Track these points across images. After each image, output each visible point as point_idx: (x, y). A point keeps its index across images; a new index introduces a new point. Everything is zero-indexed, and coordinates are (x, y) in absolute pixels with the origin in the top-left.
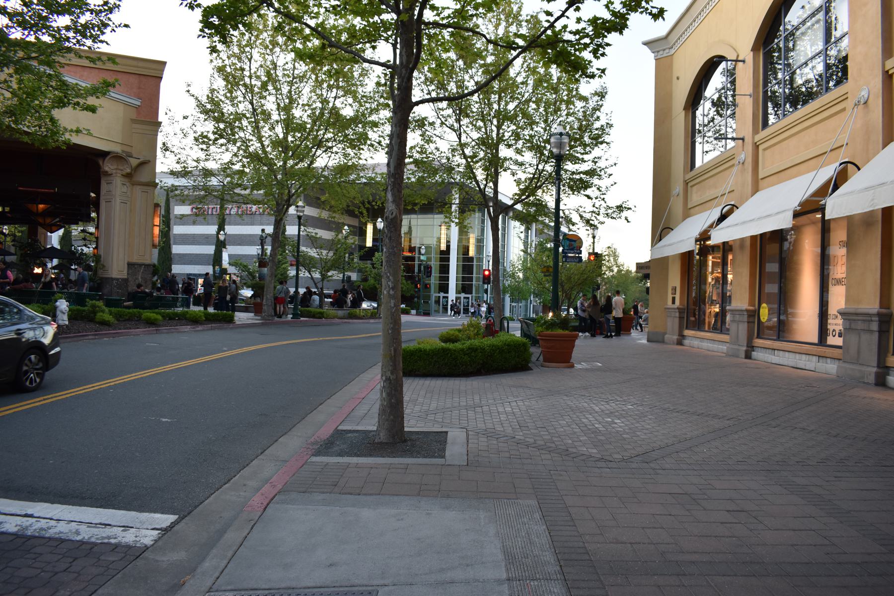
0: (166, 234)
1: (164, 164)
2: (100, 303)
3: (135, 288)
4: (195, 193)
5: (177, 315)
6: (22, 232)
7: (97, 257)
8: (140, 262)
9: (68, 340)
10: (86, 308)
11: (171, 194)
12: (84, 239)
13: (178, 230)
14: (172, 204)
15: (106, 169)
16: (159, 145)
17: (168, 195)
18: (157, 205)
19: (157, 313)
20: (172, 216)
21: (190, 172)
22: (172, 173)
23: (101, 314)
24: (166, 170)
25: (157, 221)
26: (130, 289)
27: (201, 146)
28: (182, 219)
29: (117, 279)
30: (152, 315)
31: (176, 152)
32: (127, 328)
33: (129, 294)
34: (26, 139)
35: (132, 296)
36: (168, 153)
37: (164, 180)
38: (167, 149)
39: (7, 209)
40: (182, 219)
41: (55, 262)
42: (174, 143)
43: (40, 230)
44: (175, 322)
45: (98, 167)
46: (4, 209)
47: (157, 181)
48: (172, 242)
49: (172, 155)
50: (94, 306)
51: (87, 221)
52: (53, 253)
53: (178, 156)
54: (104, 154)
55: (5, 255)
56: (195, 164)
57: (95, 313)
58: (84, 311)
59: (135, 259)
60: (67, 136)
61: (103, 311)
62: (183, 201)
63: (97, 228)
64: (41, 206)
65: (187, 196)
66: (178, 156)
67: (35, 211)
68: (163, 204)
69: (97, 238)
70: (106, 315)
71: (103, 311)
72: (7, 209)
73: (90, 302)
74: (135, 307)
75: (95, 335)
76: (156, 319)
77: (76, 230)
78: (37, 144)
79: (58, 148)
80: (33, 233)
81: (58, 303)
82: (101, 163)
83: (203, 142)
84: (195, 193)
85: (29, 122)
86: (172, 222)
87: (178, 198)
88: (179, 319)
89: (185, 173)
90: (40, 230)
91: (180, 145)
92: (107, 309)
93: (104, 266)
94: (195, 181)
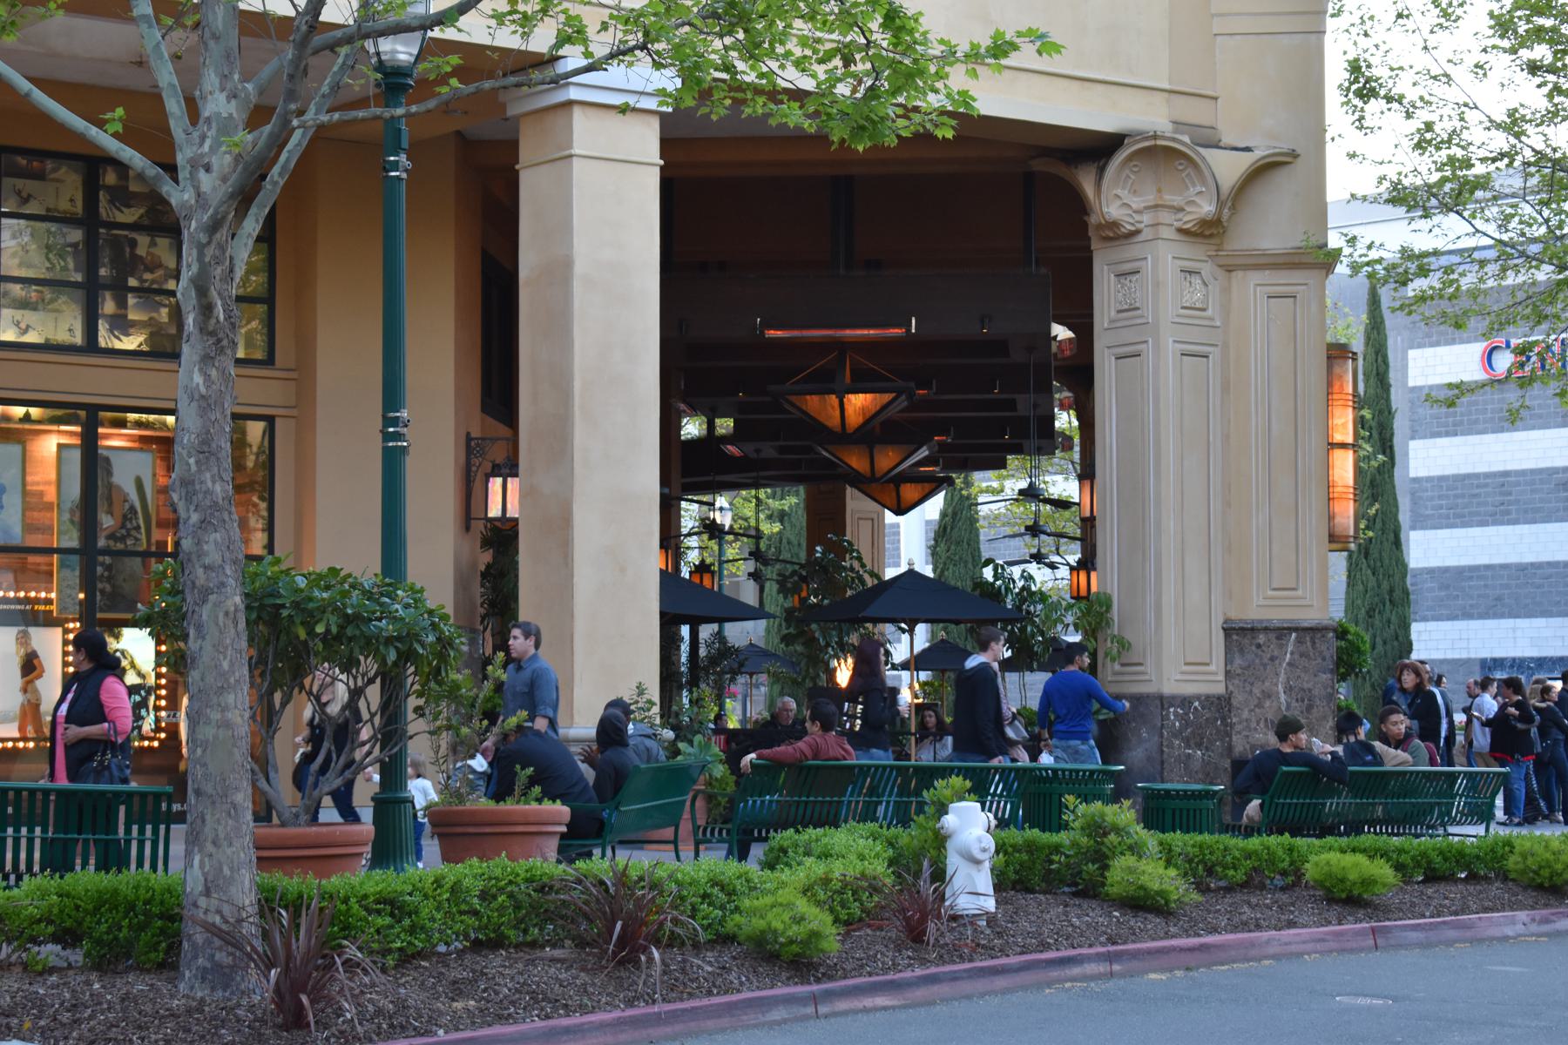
0: (1377, 484)
1: (1360, 159)
2: (1124, 814)
3: (1272, 740)
4: (1511, 280)
5: (1460, 858)
6: (782, 516)
7: (1093, 610)
8: (1278, 616)
9: (1001, 982)
10: (1063, 837)
11: (1385, 294)
12: (1034, 530)
13: (1425, 458)
14: (1394, 342)
15: (1113, 211)
16: (1335, 73)
17: (1374, 302)
18: (1337, 353)
19: (1372, 853)
20: (1397, 399)
21: (1483, 182)
22: (1403, 198)
23: (1129, 860)
24: (1370, 189)
25: (1343, 425)
26: (1240, 745)
27: (1525, 54)
28: (1451, 407)
29: (1185, 701)
30: (1349, 859)
31: (1412, 95)
32: (1244, 926)
33: (1238, 765)
34: (793, 116)
35: (1255, 774)
36: (1375, 105)
37: (1366, 234)
38: (1367, 93)
39: (725, 425)
40: (1451, 407)
41: (922, 636)
42: (1400, 54)
43: (856, 502)
44: (1454, 892)
45: (1078, 207)
46: (711, 426)
47: (1334, 241)
48: (1404, 517)
49: (1396, 115)
50: (1097, 829)
51: (1040, 451)
52: (910, 598)
53: (1423, 115)
54: (1099, 148)
55: (721, 621)
56: (1501, 141)
57: (1101, 858)
58: (1057, 849)
59: (1258, 608)
60: (958, 79)
61: (1136, 849)
62: (1451, 317)
63: (1087, 474)
64: (858, 402)
65: (1474, 294)
66: (1423, 115)
67: (833, 421)
68: (1358, 345)
69: (1088, 523)
70: (1148, 863)
71: (1136, 849)
72: (725, 425)
73: (1080, 811)
74: (1274, 824)
75: (1110, 958)
76: (1368, 882)
77: (996, 493)
78: (838, 133)
79: (924, 138)
80: (826, 520)
81: (950, 820)
82: (1089, 189)
83: (1538, 34)
84: (1511, 280)
85: (803, 41)
86: (1400, 425)
87: (1428, 310)
88: (1473, 877)
89: (1457, 192)
90: (856, 502)
91: (1422, 61)
92: (1150, 840)
93: (1124, 645)
94: (1503, 227)
